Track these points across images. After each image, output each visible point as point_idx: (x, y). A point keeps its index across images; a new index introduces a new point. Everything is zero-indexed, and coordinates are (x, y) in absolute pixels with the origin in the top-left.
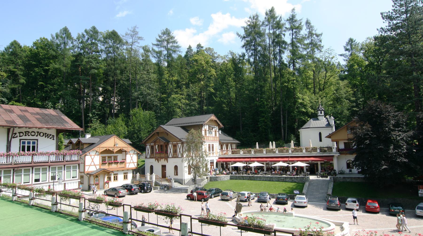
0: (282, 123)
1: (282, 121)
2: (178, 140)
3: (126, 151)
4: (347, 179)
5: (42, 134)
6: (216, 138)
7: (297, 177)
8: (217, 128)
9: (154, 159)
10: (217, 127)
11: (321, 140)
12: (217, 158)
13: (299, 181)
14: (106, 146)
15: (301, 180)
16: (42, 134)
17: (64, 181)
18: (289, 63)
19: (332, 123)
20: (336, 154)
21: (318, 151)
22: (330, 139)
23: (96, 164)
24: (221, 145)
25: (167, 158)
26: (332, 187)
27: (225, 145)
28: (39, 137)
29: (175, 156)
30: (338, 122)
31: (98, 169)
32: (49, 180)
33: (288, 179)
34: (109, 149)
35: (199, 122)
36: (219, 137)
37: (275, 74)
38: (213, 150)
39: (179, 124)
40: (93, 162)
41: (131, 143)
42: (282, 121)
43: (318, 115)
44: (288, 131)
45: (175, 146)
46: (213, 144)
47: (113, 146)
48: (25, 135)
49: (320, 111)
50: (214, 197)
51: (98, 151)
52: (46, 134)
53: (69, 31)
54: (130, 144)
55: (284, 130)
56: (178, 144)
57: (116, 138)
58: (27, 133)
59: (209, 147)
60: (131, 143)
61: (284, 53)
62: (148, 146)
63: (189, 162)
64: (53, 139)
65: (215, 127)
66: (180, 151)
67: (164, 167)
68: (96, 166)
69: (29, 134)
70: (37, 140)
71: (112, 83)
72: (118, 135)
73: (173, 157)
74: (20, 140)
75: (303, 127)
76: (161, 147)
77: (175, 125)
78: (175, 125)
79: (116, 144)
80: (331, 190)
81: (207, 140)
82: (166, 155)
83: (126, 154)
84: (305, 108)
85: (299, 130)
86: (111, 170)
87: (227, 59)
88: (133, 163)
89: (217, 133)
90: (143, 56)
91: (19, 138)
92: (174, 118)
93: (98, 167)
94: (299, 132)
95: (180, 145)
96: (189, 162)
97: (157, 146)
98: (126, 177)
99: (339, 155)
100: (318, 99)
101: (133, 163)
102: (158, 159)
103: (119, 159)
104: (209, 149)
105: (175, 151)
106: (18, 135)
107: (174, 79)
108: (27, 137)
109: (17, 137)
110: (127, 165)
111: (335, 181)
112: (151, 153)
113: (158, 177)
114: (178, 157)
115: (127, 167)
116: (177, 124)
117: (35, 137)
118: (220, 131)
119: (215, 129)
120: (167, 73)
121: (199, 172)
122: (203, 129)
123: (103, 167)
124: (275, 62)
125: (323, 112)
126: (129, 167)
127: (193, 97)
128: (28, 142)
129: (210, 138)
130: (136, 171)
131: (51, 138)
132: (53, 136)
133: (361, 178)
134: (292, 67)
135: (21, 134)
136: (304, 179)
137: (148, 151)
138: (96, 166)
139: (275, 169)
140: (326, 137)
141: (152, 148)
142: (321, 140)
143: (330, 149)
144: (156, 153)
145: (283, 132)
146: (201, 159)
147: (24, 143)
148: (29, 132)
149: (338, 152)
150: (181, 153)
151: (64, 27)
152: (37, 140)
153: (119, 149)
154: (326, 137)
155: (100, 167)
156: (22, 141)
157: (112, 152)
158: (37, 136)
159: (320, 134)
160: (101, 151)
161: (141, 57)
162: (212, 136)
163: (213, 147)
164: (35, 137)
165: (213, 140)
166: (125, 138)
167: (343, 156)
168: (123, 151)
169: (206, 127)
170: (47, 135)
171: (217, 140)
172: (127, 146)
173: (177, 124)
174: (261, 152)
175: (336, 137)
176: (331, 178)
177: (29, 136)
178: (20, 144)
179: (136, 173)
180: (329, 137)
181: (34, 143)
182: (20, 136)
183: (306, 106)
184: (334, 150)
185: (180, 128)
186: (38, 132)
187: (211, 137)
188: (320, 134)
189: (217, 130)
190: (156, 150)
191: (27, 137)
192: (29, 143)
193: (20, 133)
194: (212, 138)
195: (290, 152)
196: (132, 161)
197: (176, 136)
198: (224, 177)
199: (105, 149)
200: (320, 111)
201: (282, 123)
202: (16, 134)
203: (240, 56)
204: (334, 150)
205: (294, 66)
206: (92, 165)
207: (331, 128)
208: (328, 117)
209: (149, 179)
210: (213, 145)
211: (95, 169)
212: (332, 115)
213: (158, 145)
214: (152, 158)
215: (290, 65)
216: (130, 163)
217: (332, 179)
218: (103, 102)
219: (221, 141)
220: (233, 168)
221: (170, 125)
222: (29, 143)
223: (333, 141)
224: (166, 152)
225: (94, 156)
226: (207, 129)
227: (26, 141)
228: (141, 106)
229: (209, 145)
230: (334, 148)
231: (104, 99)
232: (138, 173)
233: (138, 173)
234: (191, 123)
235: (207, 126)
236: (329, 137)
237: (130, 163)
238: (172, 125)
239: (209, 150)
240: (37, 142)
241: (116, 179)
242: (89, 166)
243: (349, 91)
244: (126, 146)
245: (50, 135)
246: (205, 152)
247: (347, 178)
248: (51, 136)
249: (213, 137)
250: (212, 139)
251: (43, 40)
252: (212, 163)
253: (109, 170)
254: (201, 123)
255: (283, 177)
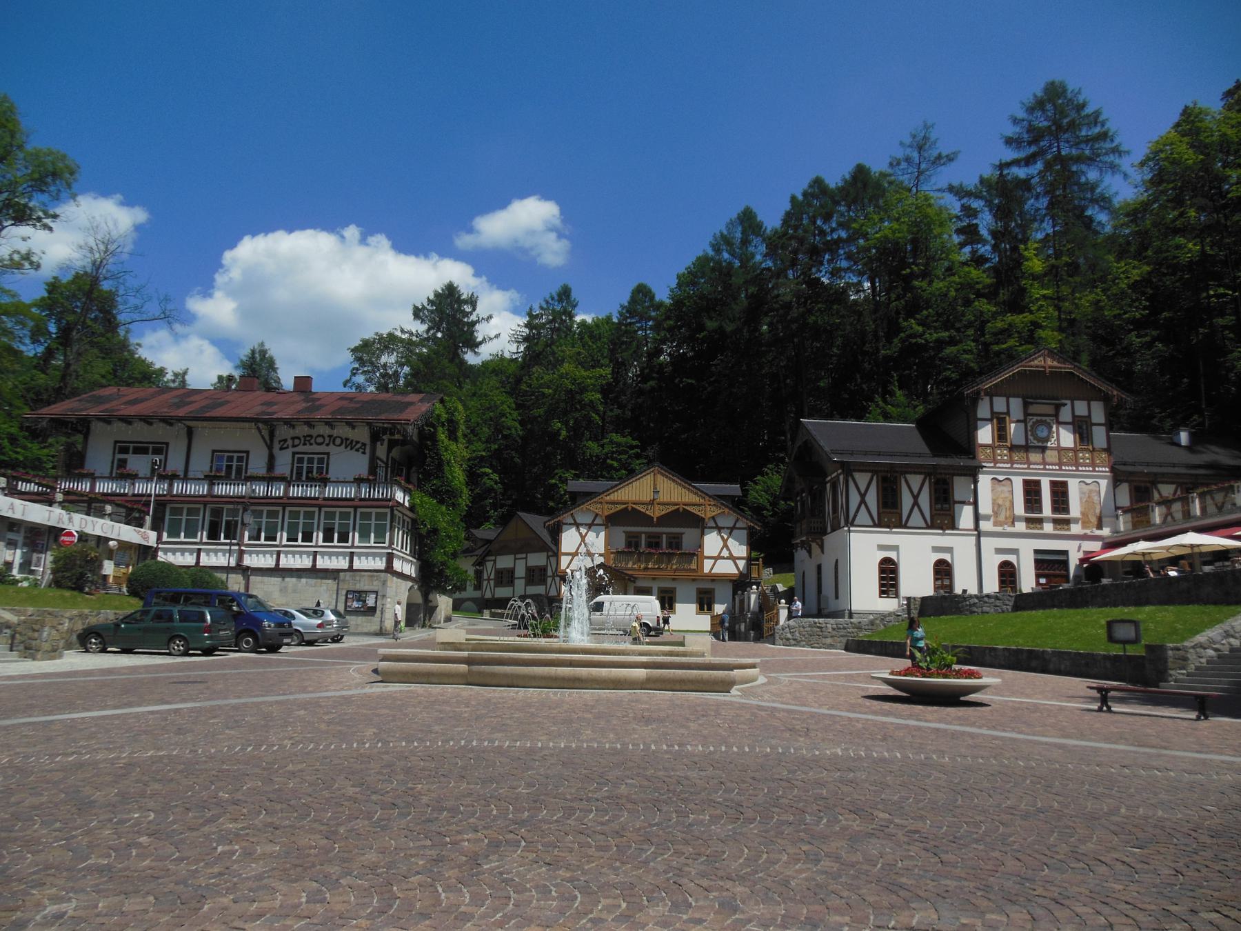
5: (338, 441)
14: (405, 418)
16: (338, 441)
17: (353, 546)
28: (332, 449)
32: (317, 541)
34: (633, 508)
48: (305, 444)
52: (347, 439)
53: (755, 217)
57: (660, 478)
58: (308, 439)
64: (364, 453)
69: (312, 441)
70: (328, 454)
74: (294, 454)
88: (731, 557)
91: (291, 450)
101: (731, 557)
106: (290, 442)
108: (307, 448)
109: (287, 447)
115: (706, 570)
117: (323, 448)
128: (309, 459)
131: (357, 450)
132: (364, 445)
133: (1201, 503)
135: (297, 442)
147: (301, 461)
148: (311, 436)
151: (741, 209)
152: (328, 454)
156: (297, 456)
157: (645, 520)
158: (328, 445)
164: (323, 448)
170: (350, 444)
177: (311, 444)
178: (293, 464)
181: (321, 461)
182: (294, 446)
186: (330, 436)
191: (307, 448)
192: (311, 461)
193: (293, 439)
196: (725, 553)
199: (620, 507)
202: (285, 440)
222: (311, 461)
227: (306, 457)
240: (328, 458)
244: (697, 500)
245: (357, 442)
248: (359, 446)
251: (698, 259)
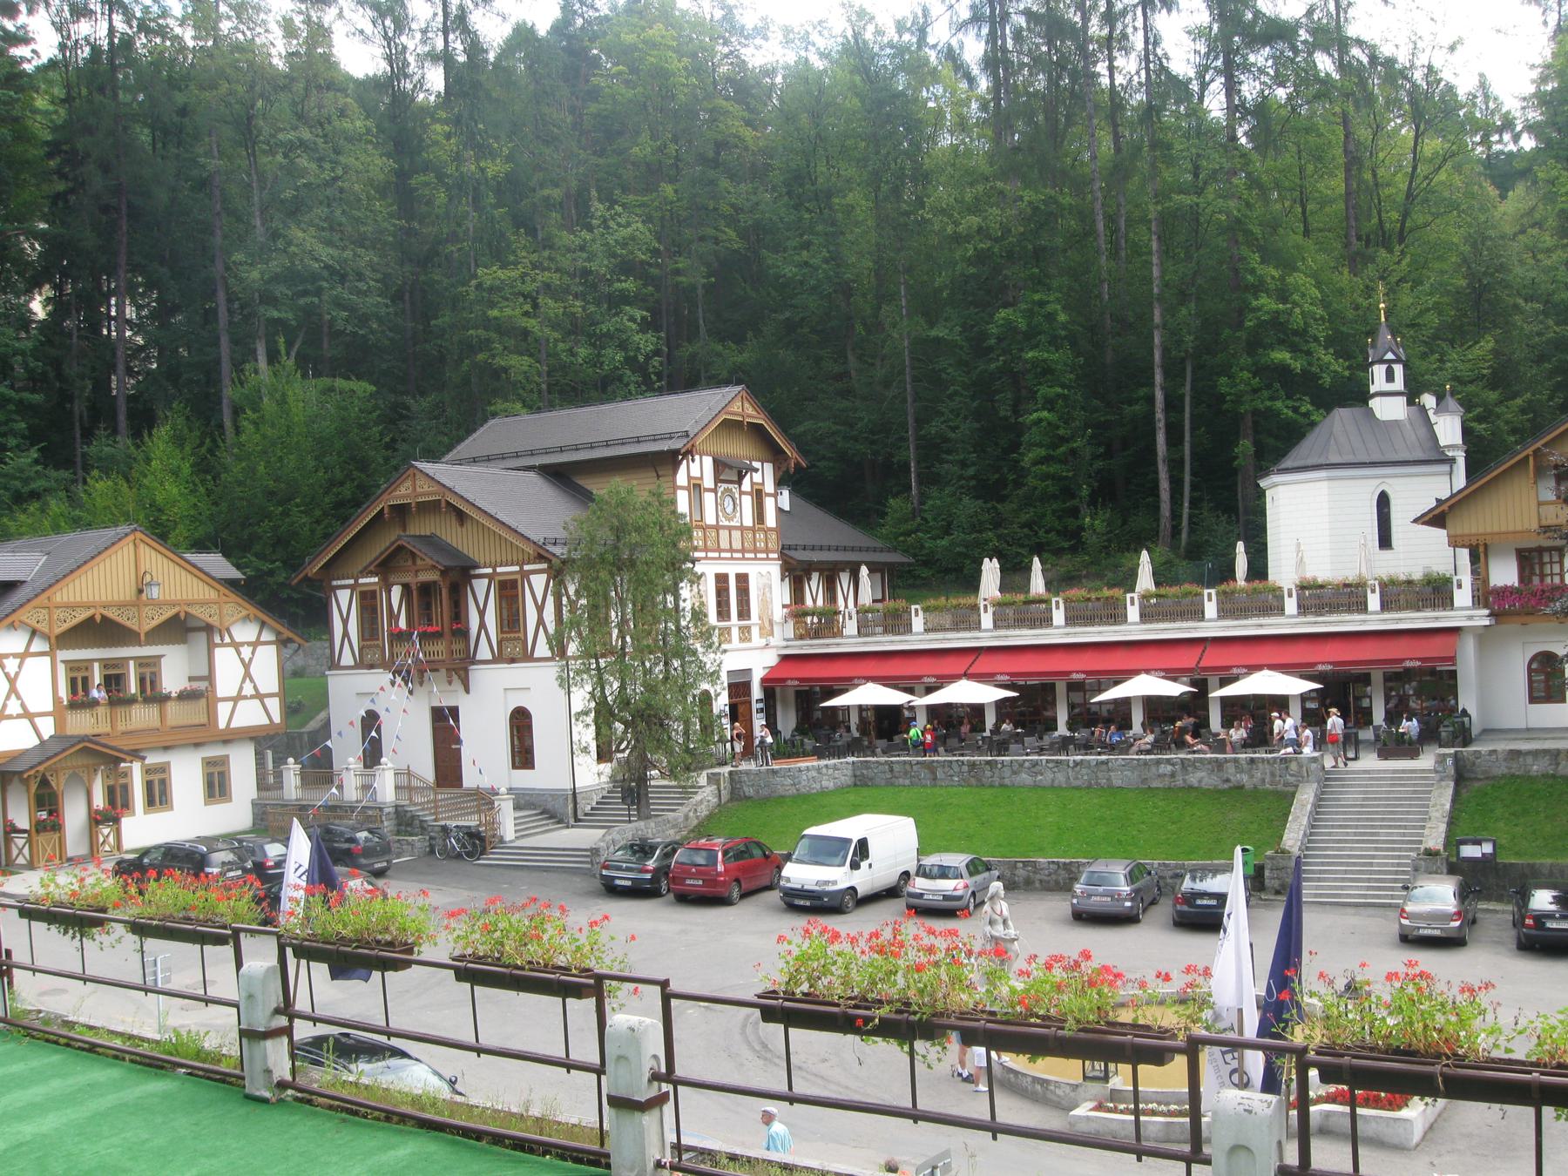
0: (1161, 438)
1: (1161, 425)
2: (530, 550)
3: (209, 629)
4: (1530, 760)
6: (760, 536)
7: (1252, 761)
8: (764, 475)
9: (382, 677)
10: (769, 468)
11: (1385, 541)
12: (771, 659)
13: (1263, 781)
15: (1273, 775)
18: (1201, 75)
19: (1449, 430)
20: (1470, 618)
21: (1374, 601)
22: (1439, 535)
23: (263, 690)
24: (796, 574)
25: (460, 668)
26: (1448, 806)
27: (815, 576)
29: (513, 649)
30: (1480, 428)
31: (46, 737)
33: (1199, 774)
34: (104, 618)
35: (655, 438)
36: (779, 529)
37: (1117, 137)
38: (744, 613)
39: (532, 453)
40: (18, 697)
41: (235, 574)
42: (1161, 425)
43: (1373, 389)
44: (1194, 487)
45: (509, 593)
46: (742, 569)
47: (127, 593)
49: (1384, 367)
50: (745, 895)
51: (44, 627)
54: (232, 584)
55: (1176, 483)
56: (525, 575)
59: (722, 591)
60: (235, 574)
61: (1169, 11)
62: (344, 596)
63: (601, 683)
65: (757, 465)
66: (541, 622)
67: (445, 723)
68: (37, 720)
71: (105, 209)
72: (160, 531)
73: (498, 658)
75: (1283, 466)
76: (421, 597)
77: (503, 457)
78: (503, 457)
79: (149, 584)
80: (1443, 827)
81: (706, 550)
82: (455, 647)
83: (211, 647)
84: (1294, 349)
85: (1263, 483)
86: (126, 744)
87: (821, 43)
88: (259, 696)
89: (769, 504)
90: (289, 30)
91: (325, 381)
92: (494, 415)
93: (47, 727)
94: (1261, 494)
95: (539, 581)
96: (601, 683)
97: (396, 592)
98: (217, 786)
99: (1487, 623)
100: (1369, 291)
101: (259, 696)
102: (412, 676)
103: (173, 679)
104: (719, 604)
105: (511, 620)
107: (490, 173)
110: (223, 710)
111: (1462, 775)
112: (363, 636)
113: (415, 783)
114: (528, 657)
115: (222, 725)
116: (517, 455)
118: (786, 493)
119: (757, 477)
120: (448, 136)
121: (663, 744)
122: (681, 478)
123: (82, 724)
124: (1120, 62)
125: (1398, 370)
126: (232, 726)
127: (610, 282)
129: (724, 534)
130: (274, 748)
134: (1222, 97)
136: (1294, 766)
137: (345, 622)
138: (37, 720)
139: (1119, 713)
140: (1416, 521)
141: (368, 604)
142: (1385, 541)
143: (1437, 591)
144: (391, 635)
145: (1164, 485)
146: (676, 663)
149: (1486, 606)
150: (551, 628)
153: (169, 613)
154: (1416, 521)
155: (60, 723)
159: (1383, 501)
160: (58, 631)
161: (277, 34)
162: (736, 523)
163: (743, 591)
165: (743, 551)
166: (200, 546)
167: (1511, 627)
168: (192, 624)
169: (701, 468)
171: (767, 551)
172: (213, 595)
173: (517, 455)
174: (895, 622)
175: (1484, 521)
176: (1444, 756)
179: (279, 761)
180: (1436, 518)
183: (1302, 333)
184: (1463, 597)
185: (532, 476)
187: (730, 529)
188: (1383, 501)
189: (769, 487)
190: (393, 617)
194: (736, 534)
195: (1133, 613)
197: (513, 524)
198: (819, 770)
199: (82, 616)
200: (1384, 367)
201: (1161, 438)
203: (900, 27)
204: (1463, 596)
205: (1231, 88)
206: (245, 698)
207: (1446, 468)
208: (1429, 400)
209: (351, 790)
210: (743, 579)
211: (30, 741)
212: (1453, 394)
213: (406, 588)
214: (371, 667)
215: (1204, 86)
216: (239, 698)
217: (1449, 761)
218: (51, 327)
219: (792, 553)
220: (870, 715)
221: (474, 461)
223: (1454, 543)
224: (461, 632)
225: (23, 656)
226: (709, 482)
228: (288, 354)
229: (722, 579)
230: (1460, 586)
231: (59, 307)
232: (291, 760)
233: (291, 760)
234: (607, 444)
235: (708, 462)
236: (1436, 518)
237: (239, 698)
238: (489, 459)
239: (723, 613)
241: (158, 796)
242: (266, 700)
243: (1548, 251)
246: (698, 615)
247: (1529, 753)
249: (742, 528)
250: (737, 545)
252: (739, 688)
253: (103, 741)
254: (665, 446)
255: (1168, 761)
